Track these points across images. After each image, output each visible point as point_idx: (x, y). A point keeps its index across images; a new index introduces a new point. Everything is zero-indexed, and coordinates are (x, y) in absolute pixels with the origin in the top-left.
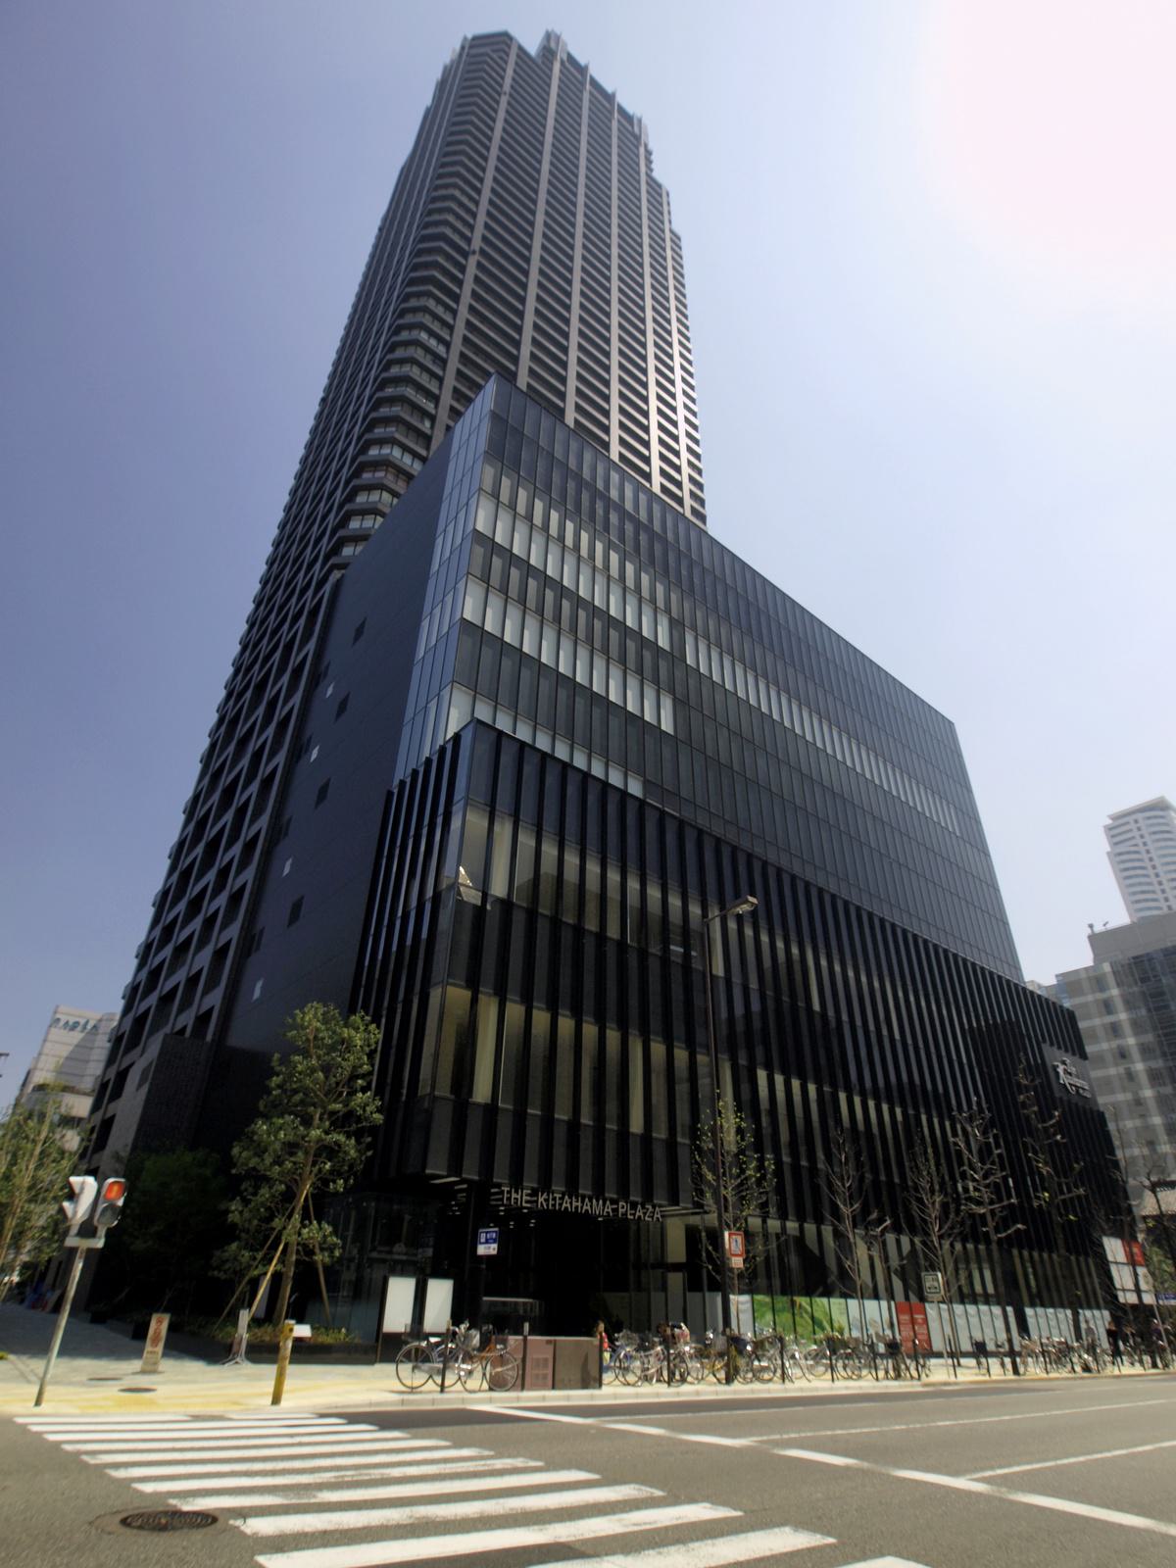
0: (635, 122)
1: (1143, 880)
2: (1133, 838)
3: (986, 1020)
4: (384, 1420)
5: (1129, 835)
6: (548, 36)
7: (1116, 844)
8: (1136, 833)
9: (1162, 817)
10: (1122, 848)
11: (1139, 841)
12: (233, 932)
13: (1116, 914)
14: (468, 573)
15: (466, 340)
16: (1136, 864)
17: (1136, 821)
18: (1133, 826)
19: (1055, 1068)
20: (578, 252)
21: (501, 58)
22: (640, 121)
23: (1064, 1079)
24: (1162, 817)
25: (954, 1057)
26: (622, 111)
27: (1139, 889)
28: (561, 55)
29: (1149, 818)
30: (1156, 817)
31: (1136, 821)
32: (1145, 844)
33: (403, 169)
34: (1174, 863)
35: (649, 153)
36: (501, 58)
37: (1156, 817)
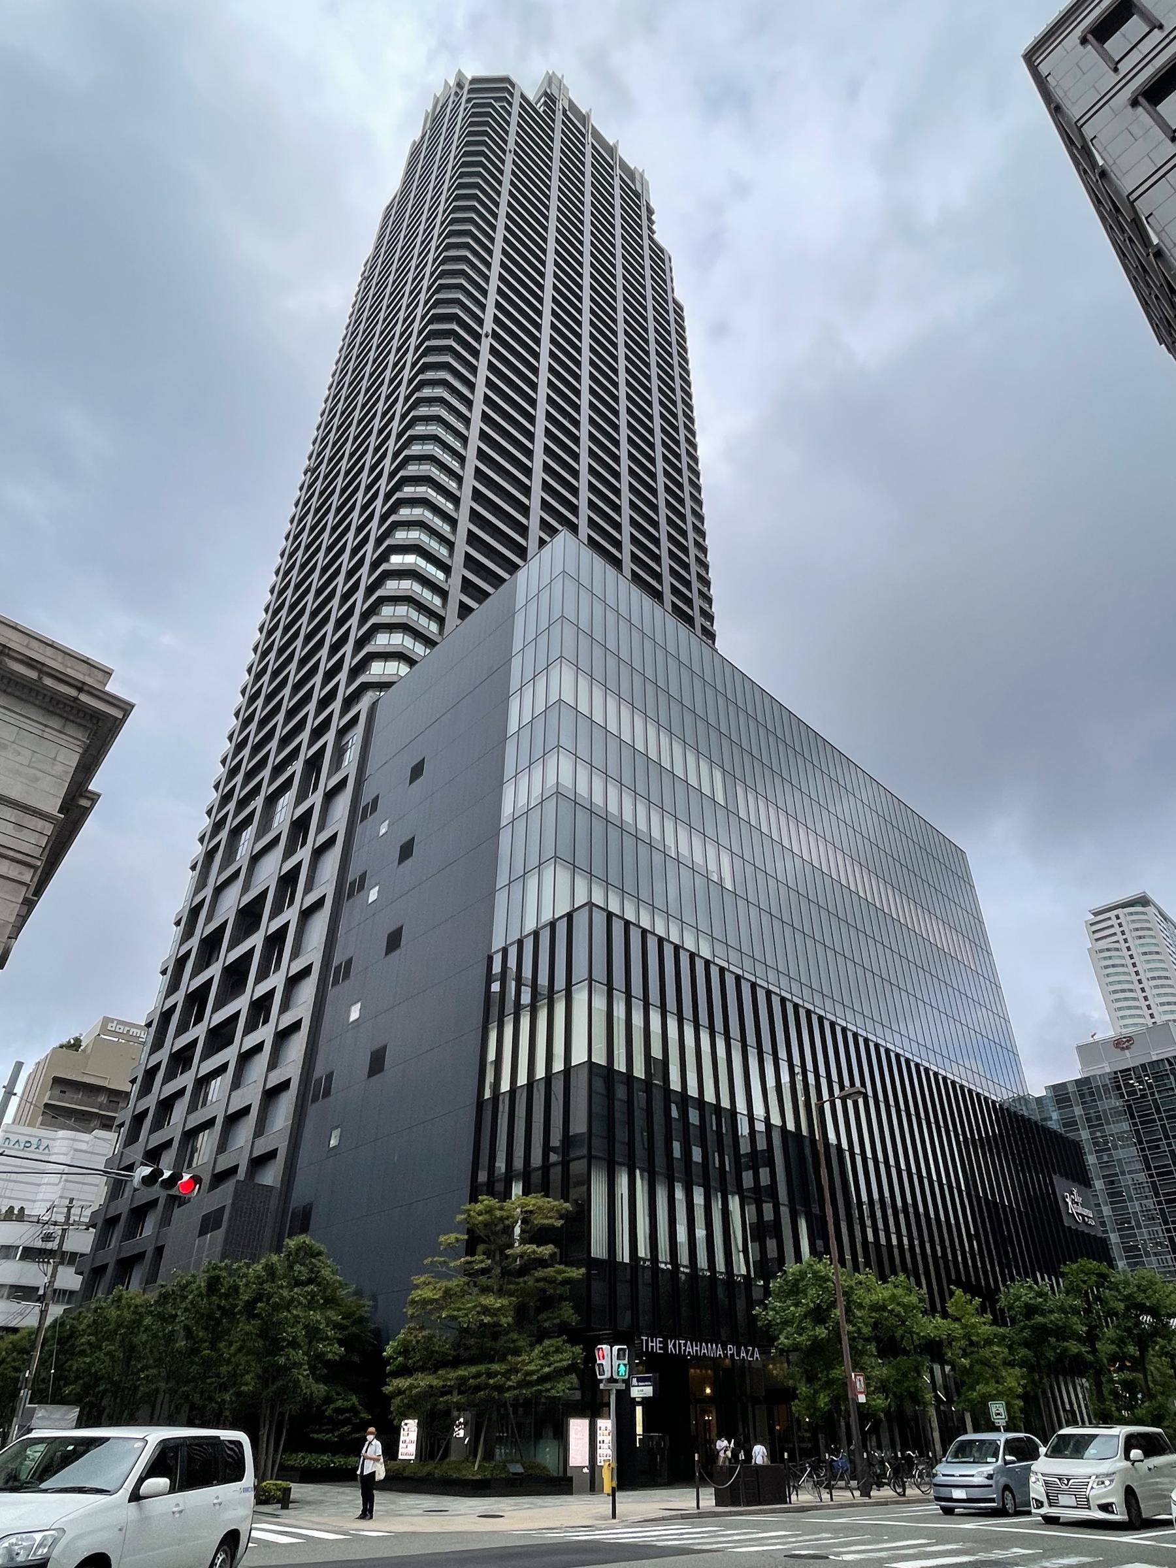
0: (637, 176)
1: (1133, 1012)
2: (1115, 934)
3: (993, 1131)
4: (685, 1517)
5: (1111, 931)
6: (550, 79)
7: (1097, 940)
8: (1117, 929)
9: (1143, 913)
10: (1103, 944)
11: (1120, 937)
12: (313, 953)
13: (1103, 1025)
14: (558, 746)
15: (483, 434)
16: (1133, 1012)
17: (1118, 917)
18: (1114, 922)
19: (1064, 1198)
20: (505, 188)
21: (503, 107)
22: (642, 176)
23: (1072, 1209)
24: (1143, 913)
25: (932, 1120)
26: (624, 166)
27: (1119, 987)
28: (562, 104)
29: (1131, 914)
30: (1136, 913)
31: (1118, 917)
32: (1126, 941)
33: (390, 208)
34: (1172, 1012)
35: (650, 212)
36: (503, 107)
37: (1136, 913)
